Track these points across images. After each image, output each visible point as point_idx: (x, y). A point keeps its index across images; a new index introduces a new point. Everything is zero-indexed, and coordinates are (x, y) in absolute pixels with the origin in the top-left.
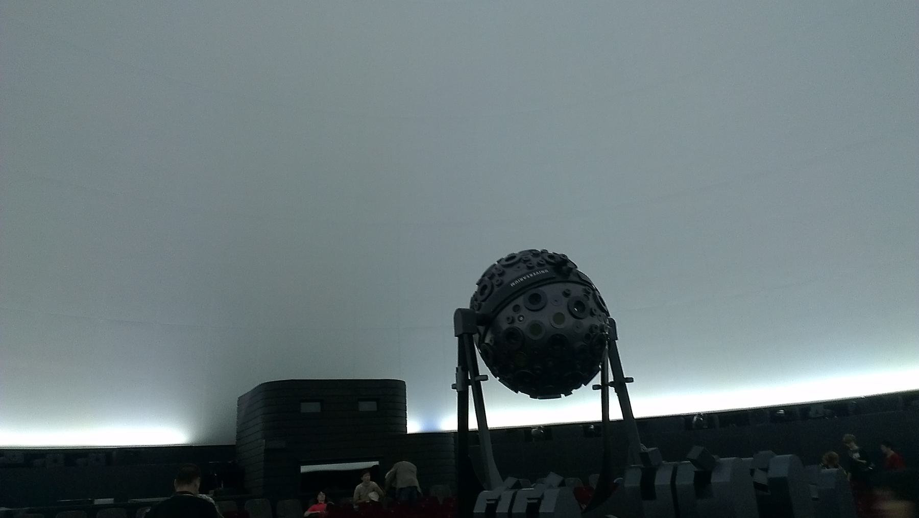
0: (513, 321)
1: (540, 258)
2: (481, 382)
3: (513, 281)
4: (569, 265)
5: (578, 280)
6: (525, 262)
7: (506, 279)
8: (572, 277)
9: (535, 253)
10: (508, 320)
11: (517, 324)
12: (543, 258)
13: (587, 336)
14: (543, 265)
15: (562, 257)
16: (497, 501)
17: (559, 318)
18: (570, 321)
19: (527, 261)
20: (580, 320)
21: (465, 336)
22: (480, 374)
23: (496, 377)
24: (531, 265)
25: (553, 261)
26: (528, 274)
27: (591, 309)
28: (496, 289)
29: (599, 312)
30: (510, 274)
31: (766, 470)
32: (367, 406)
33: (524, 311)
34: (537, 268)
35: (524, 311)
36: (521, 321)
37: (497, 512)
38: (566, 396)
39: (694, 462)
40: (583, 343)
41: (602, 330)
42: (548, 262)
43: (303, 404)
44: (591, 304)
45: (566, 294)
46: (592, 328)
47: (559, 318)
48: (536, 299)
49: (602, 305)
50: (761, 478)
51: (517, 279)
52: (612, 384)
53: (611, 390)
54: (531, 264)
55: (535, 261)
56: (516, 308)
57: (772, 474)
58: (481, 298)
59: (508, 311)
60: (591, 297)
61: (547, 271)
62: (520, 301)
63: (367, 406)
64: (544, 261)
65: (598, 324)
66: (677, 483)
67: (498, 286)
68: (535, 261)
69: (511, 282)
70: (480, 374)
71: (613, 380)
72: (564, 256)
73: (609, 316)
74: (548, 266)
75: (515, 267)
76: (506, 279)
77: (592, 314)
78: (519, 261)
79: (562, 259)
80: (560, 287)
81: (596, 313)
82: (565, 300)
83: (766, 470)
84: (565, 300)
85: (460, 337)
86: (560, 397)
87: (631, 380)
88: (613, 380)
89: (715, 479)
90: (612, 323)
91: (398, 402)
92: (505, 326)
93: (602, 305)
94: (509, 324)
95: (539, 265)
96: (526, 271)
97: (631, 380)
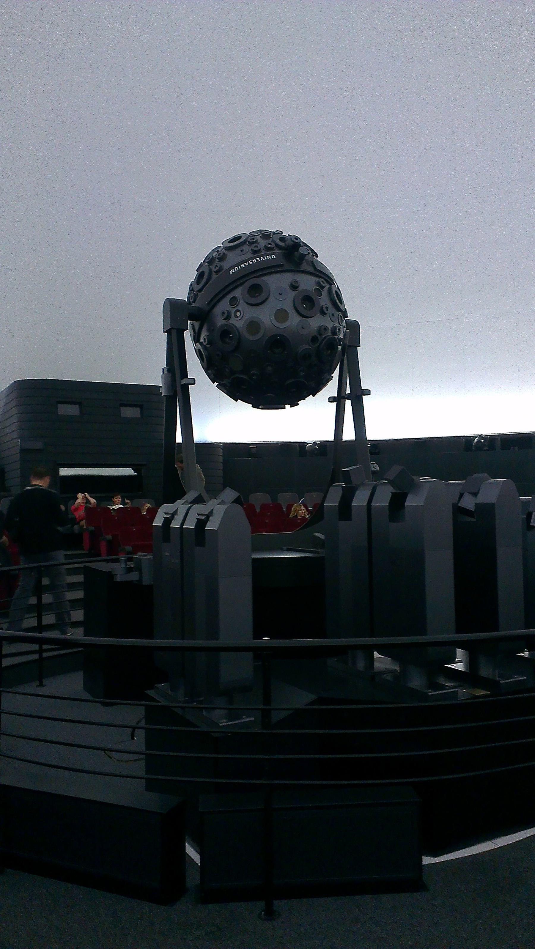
0: (228, 317)
1: (270, 241)
2: (189, 386)
3: (233, 267)
4: (302, 250)
5: (311, 269)
6: (251, 243)
7: (226, 265)
8: (305, 266)
9: (266, 235)
10: (222, 315)
11: (233, 321)
12: (273, 241)
13: (314, 339)
14: (272, 249)
15: (294, 240)
16: (208, 516)
17: (281, 315)
18: (294, 320)
19: (253, 243)
20: (307, 319)
21: (174, 333)
22: (189, 377)
23: (214, 383)
24: (256, 249)
25: (283, 244)
26: (251, 259)
27: (322, 307)
28: (214, 276)
29: (331, 310)
30: (232, 257)
31: (475, 494)
32: (129, 412)
33: (242, 306)
34: (263, 252)
35: (242, 306)
36: (238, 317)
37: (352, 504)
38: (291, 407)
39: (391, 482)
40: (308, 347)
41: (334, 333)
42: (277, 245)
43: (60, 406)
44: (324, 300)
45: (294, 287)
46: (322, 330)
47: (281, 315)
48: (255, 289)
49: (339, 303)
50: (468, 502)
51: (237, 265)
52: (349, 397)
53: (348, 404)
54: (257, 247)
55: (262, 243)
56: (234, 302)
57: (482, 499)
58: (197, 287)
59: (224, 305)
60: (324, 293)
61: (273, 256)
62: (238, 293)
63: (129, 412)
64: (273, 244)
65: (330, 326)
66: (373, 504)
67: (217, 272)
68: (262, 243)
69: (230, 269)
70: (189, 377)
71: (349, 392)
72: (297, 238)
73: (347, 317)
74: (277, 251)
75: (238, 251)
76: (226, 265)
77: (323, 313)
78: (244, 242)
79: (293, 241)
80: (286, 279)
81: (326, 312)
82: (292, 294)
83: (475, 494)
84: (292, 294)
85: (168, 332)
86: (285, 408)
87: (368, 393)
88: (349, 392)
89: (411, 501)
90: (354, 327)
91: (18, 405)
92: (220, 322)
93: (339, 303)
94: (223, 319)
95: (267, 249)
96: (249, 255)
97: (368, 393)
